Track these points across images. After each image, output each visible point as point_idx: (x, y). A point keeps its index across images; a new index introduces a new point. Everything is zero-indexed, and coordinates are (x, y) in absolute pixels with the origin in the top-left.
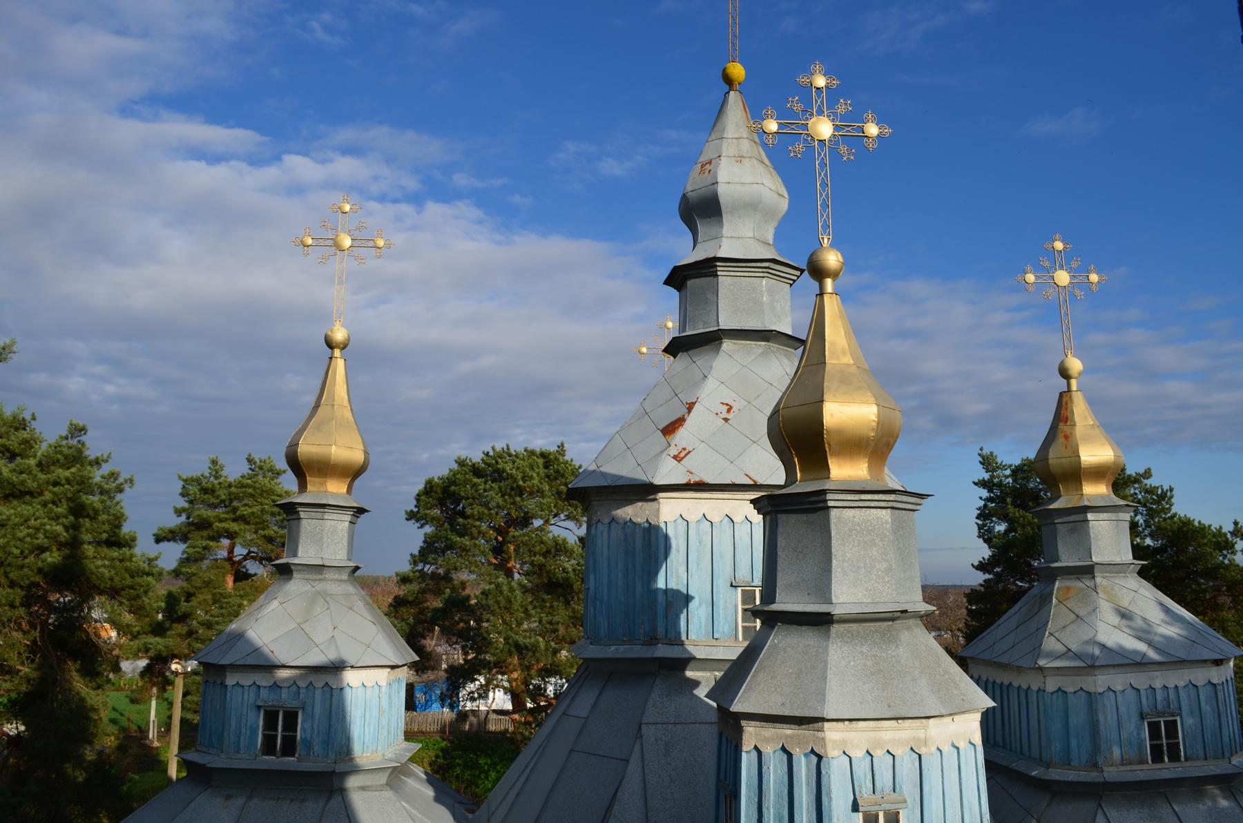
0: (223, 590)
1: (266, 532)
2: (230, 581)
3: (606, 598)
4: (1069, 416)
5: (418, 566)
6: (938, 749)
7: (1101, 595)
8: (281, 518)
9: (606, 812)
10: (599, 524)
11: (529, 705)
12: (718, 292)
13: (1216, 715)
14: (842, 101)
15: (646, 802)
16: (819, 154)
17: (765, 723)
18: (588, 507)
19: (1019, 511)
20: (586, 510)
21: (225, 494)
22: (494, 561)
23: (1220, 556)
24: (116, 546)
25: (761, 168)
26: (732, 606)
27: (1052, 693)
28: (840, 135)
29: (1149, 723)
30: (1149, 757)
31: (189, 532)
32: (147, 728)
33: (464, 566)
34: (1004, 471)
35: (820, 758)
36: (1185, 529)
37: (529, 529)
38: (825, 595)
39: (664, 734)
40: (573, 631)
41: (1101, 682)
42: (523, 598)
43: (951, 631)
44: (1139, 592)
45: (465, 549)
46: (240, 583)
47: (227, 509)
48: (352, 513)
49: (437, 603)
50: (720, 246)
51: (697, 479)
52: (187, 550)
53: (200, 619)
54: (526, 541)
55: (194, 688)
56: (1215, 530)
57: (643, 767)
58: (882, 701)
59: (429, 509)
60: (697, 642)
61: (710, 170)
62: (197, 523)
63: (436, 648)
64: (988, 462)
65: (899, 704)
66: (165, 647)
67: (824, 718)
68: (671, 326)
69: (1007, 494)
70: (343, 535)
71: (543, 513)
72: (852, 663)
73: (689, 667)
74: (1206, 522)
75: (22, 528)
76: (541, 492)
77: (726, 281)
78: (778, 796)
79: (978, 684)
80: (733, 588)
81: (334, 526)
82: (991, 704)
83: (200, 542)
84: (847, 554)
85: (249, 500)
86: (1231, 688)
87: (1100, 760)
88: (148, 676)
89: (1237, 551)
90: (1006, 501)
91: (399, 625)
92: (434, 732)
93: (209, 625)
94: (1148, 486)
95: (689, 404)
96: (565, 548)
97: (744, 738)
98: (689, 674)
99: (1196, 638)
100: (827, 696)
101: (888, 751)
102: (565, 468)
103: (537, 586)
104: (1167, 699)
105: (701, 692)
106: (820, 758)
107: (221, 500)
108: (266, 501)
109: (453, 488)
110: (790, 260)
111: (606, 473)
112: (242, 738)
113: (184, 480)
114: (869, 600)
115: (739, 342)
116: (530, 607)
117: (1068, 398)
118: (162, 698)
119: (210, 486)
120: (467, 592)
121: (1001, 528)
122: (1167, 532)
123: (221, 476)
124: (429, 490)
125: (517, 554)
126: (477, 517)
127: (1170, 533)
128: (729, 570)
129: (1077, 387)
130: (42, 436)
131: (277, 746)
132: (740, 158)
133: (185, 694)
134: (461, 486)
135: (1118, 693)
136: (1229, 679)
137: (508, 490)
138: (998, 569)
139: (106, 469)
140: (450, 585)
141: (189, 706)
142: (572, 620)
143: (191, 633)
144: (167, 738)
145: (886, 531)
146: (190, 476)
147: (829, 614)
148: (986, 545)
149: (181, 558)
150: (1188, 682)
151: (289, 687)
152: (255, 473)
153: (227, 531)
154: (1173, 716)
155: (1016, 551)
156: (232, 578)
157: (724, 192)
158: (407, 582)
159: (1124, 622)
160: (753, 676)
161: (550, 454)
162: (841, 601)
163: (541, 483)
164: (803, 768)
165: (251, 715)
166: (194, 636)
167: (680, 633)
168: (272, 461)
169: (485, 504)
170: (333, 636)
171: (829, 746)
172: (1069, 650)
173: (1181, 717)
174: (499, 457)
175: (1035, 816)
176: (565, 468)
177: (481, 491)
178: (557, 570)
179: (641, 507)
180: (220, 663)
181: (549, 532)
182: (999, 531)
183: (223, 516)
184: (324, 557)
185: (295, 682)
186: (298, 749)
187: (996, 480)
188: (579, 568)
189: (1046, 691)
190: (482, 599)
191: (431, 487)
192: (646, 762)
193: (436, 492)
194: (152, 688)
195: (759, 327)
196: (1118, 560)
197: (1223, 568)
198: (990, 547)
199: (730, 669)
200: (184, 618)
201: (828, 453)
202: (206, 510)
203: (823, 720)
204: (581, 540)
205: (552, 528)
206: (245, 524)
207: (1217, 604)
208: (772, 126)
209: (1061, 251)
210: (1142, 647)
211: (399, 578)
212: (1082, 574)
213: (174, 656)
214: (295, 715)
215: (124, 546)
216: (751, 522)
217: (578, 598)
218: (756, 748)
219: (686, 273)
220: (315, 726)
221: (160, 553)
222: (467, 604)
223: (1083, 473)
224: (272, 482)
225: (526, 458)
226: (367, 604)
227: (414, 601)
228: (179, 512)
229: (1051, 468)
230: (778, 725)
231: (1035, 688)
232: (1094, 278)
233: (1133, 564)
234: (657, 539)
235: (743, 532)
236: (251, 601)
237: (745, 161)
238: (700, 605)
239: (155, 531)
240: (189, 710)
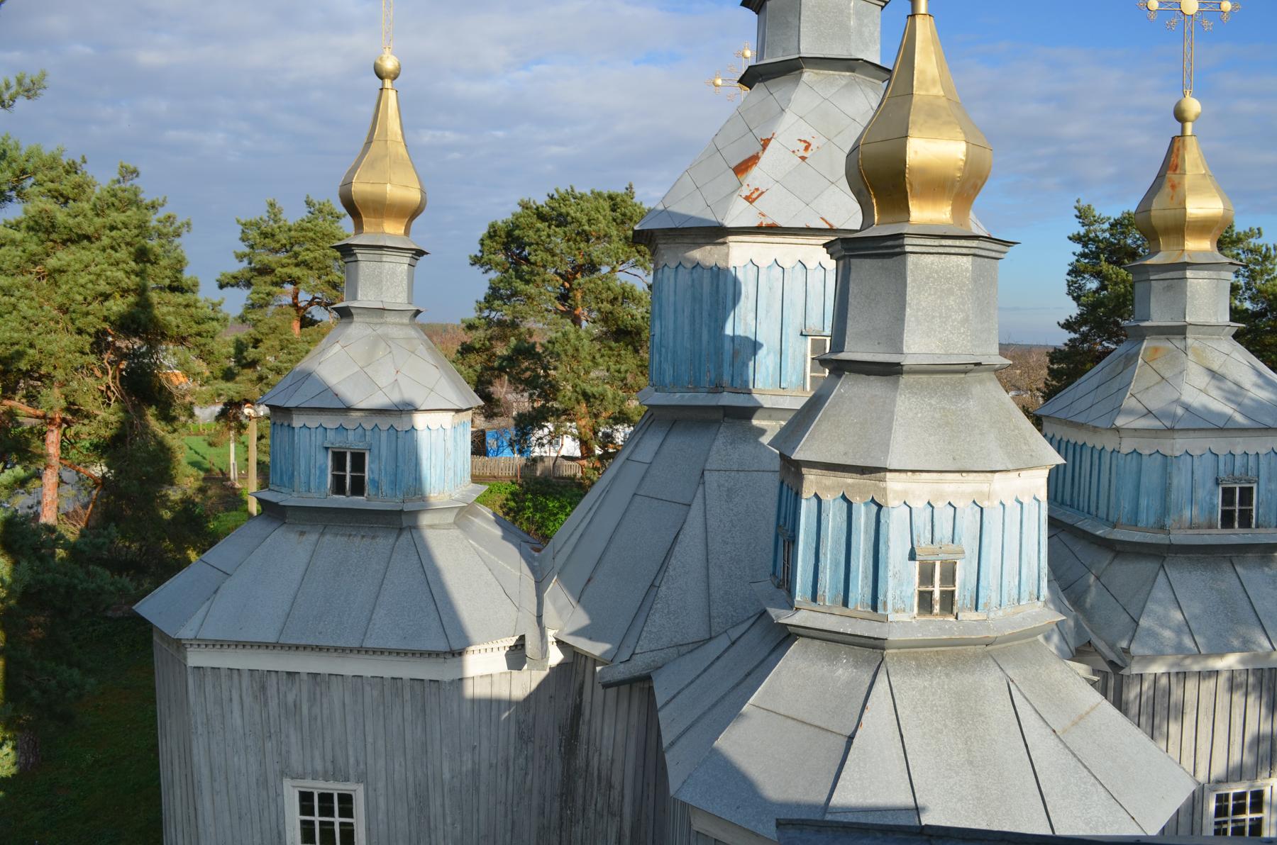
1: (329, 278)
2: (296, 325)
3: (671, 344)
6: (1001, 503)
9: (667, 554)
10: (666, 268)
12: (800, 14)
15: (707, 545)
18: (654, 251)
22: (561, 308)
24: (178, 291)
26: (800, 356)
27: (1127, 455)
29: (1224, 490)
30: (1219, 523)
35: (880, 507)
38: (898, 348)
41: (1178, 445)
43: (1031, 391)
44: (1232, 355)
47: (288, 254)
48: (410, 255)
49: (501, 350)
51: (770, 222)
52: (251, 296)
57: (705, 512)
60: (764, 390)
62: (259, 269)
68: (749, 56)
70: (403, 278)
73: (755, 416)
75: (83, 273)
78: (836, 542)
79: (1051, 444)
87: (1169, 522)
91: (465, 372)
92: (505, 477)
93: (278, 371)
94: (1252, 246)
97: (804, 486)
98: (755, 422)
101: (950, 503)
105: (765, 440)
106: (880, 507)
112: (312, 478)
113: (242, 225)
115: (821, 72)
116: (598, 356)
117: (1180, 144)
121: (1093, 285)
127: (1271, 297)
128: (800, 319)
129: (1192, 132)
130: (95, 179)
131: (345, 483)
133: (260, 438)
137: (573, 235)
139: (162, 213)
140: (516, 332)
141: (264, 449)
142: (640, 369)
143: (261, 379)
145: (965, 280)
146: (248, 220)
147: (898, 364)
148: (1074, 304)
156: (299, 324)
159: (1214, 382)
160: (817, 425)
161: (618, 195)
164: (863, 516)
166: (265, 381)
167: (747, 382)
170: (396, 380)
171: (890, 496)
173: (1258, 484)
175: (1094, 572)
179: (710, 251)
181: (615, 280)
186: (367, 489)
191: (495, 231)
192: (708, 507)
195: (845, 55)
196: (1213, 321)
198: (1079, 305)
199: (795, 417)
200: (253, 364)
203: (885, 470)
204: (650, 287)
205: (619, 275)
210: (1228, 409)
211: (464, 325)
212: (1174, 334)
213: (247, 401)
214: (363, 455)
215: (187, 291)
218: (816, 495)
221: (223, 299)
227: (480, 348)
228: (240, 257)
229: (1154, 223)
234: (725, 284)
235: (816, 278)
238: (768, 354)
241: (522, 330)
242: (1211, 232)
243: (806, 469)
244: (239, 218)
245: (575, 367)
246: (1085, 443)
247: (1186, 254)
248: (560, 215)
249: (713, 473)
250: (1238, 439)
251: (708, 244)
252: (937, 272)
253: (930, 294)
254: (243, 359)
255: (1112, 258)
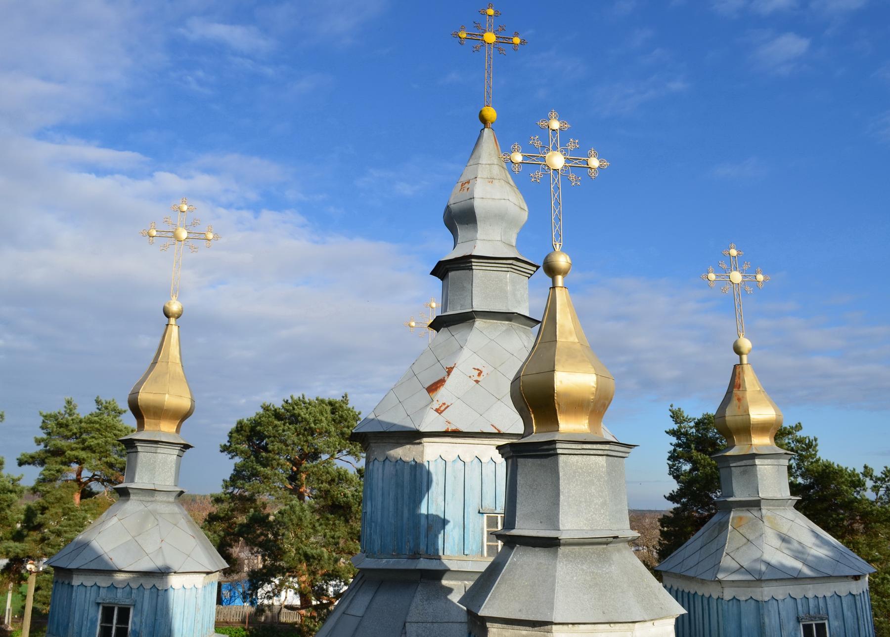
0: (71, 505)
1: (108, 459)
2: (77, 497)
3: (379, 520)
4: (741, 384)
5: (229, 489)
7: (766, 523)
8: (120, 448)
10: (376, 461)
11: (314, 603)
12: (472, 282)
13: (856, 620)
14: (571, 140)
16: (554, 180)
17: (506, 625)
19: (700, 455)
20: (365, 448)
21: (76, 428)
22: (290, 487)
23: (855, 492)
25: (508, 188)
26: (479, 528)
27: (728, 601)
28: (570, 166)
29: (804, 626)
31: (46, 458)
32: (3, 614)
33: (265, 491)
34: (689, 423)
36: (827, 471)
37: (318, 461)
39: (424, 631)
40: (351, 545)
41: (766, 592)
42: (312, 517)
43: (647, 547)
45: (266, 477)
46: (85, 500)
47: (77, 440)
48: (179, 448)
49: (242, 519)
50: (475, 246)
52: (44, 472)
53: (52, 528)
54: (315, 471)
55: (43, 584)
56: (850, 472)
58: (598, 609)
59: (239, 444)
61: (468, 189)
63: (240, 554)
64: (676, 416)
65: (612, 611)
66: (22, 551)
67: (552, 622)
68: (435, 308)
69: (692, 441)
71: (329, 449)
72: (575, 578)
73: (444, 577)
74: (831, 460)
76: (328, 433)
77: (479, 273)
79: (670, 593)
80: (480, 515)
81: (164, 458)
82: (684, 611)
83: (54, 466)
84: (572, 491)
85: (96, 434)
86: (866, 598)
88: (7, 573)
89: (867, 488)
90: (690, 446)
91: (212, 537)
92: (236, 623)
93: (59, 534)
94: (798, 437)
95: (449, 368)
96: (346, 478)
98: (445, 582)
99: (840, 558)
100: (555, 604)
102: (348, 414)
103: (323, 507)
104: (818, 606)
105: (455, 597)
107: (73, 433)
108: (109, 435)
109: (258, 428)
110: (528, 259)
111: (382, 422)
114: (589, 528)
115: (488, 321)
116: (317, 524)
117: (740, 370)
118: (18, 591)
119: (65, 422)
120: (267, 511)
121: (687, 467)
122: (814, 473)
123: (74, 414)
124: (239, 429)
125: (308, 481)
126: (276, 452)
127: (816, 474)
131: (111, 634)
132: (491, 180)
133: (37, 589)
134: (265, 427)
135: (779, 602)
136: (865, 591)
137: (302, 431)
138: (684, 500)
140: (253, 505)
141: (39, 599)
143: (43, 540)
144: (20, 624)
146: (49, 413)
147: (557, 538)
148: (675, 481)
149: (38, 479)
150: (834, 593)
151: (123, 588)
152: (101, 412)
153: (77, 458)
154: (823, 620)
155: (698, 485)
156: (79, 496)
157: (479, 206)
158: (219, 502)
159: (784, 545)
160: (497, 587)
161: (336, 402)
162: (567, 528)
163: (328, 426)
165: (92, 610)
167: (437, 550)
168: (115, 403)
169: (283, 441)
172: (742, 567)
173: (829, 620)
174: (296, 404)
176: (348, 414)
177: (280, 431)
178: (339, 495)
180: (67, 568)
182: (686, 470)
183: (74, 446)
184: (156, 483)
185: (128, 584)
187: (683, 430)
188: (357, 494)
189: (724, 599)
190: (279, 517)
191: (242, 427)
193: (245, 431)
194: (9, 583)
195: (503, 309)
196: (779, 496)
197: (857, 502)
198: (678, 482)
201: (557, 411)
202: (60, 441)
203: (552, 623)
204: (359, 471)
205: (336, 461)
206: (92, 452)
207: (853, 529)
208: (518, 157)
209: (735, 257)
210: (798, 565)
211: (213, 498)
213: (29, 557)
216: (495, 462)
217: (355, 517)
219: (448, 266)
220: (143, 621)
221: (23, 475)
222: (267, 521)
223: (752, 427)
224: (115, 420)
225: (317, 406)
226: (189, 521)
227: (224, 517)
228: (38, 442)
229: (728, 423)
230: (516, 627)
231: (715, 596)
232: (760, 277)
233: (791, 499)
234: (421, 474)
236: (95, 516)
237: (495, 182)
238: (454, 528)
239: (19, 456)
240: (39, 602)
241: (258, 503)
242: (769, 431)
243: (489, 624)
244: (42, 411)
245: (299, 534)
246: (696, 592)
247: (753, 447)
248: (293, 415)
249: (413, 624)
250: (809, 586)
251: (408, 444)
252: (581, 468)
253: (577, 485)
254: (31, 522)
255: (698, 447)
